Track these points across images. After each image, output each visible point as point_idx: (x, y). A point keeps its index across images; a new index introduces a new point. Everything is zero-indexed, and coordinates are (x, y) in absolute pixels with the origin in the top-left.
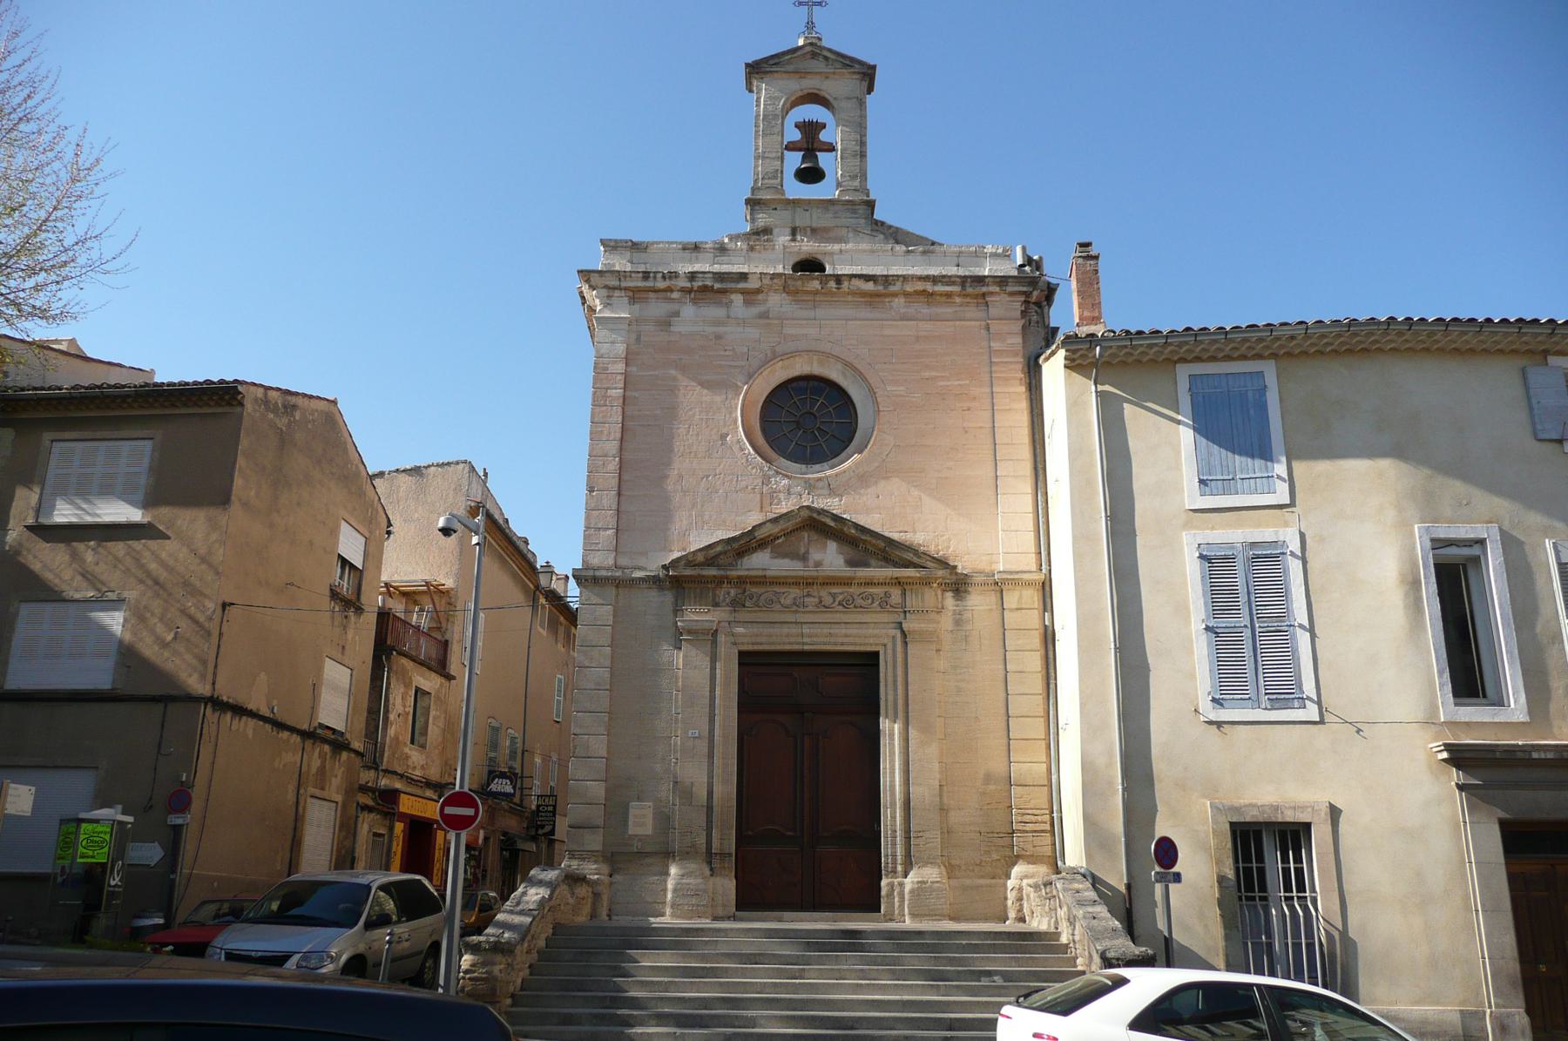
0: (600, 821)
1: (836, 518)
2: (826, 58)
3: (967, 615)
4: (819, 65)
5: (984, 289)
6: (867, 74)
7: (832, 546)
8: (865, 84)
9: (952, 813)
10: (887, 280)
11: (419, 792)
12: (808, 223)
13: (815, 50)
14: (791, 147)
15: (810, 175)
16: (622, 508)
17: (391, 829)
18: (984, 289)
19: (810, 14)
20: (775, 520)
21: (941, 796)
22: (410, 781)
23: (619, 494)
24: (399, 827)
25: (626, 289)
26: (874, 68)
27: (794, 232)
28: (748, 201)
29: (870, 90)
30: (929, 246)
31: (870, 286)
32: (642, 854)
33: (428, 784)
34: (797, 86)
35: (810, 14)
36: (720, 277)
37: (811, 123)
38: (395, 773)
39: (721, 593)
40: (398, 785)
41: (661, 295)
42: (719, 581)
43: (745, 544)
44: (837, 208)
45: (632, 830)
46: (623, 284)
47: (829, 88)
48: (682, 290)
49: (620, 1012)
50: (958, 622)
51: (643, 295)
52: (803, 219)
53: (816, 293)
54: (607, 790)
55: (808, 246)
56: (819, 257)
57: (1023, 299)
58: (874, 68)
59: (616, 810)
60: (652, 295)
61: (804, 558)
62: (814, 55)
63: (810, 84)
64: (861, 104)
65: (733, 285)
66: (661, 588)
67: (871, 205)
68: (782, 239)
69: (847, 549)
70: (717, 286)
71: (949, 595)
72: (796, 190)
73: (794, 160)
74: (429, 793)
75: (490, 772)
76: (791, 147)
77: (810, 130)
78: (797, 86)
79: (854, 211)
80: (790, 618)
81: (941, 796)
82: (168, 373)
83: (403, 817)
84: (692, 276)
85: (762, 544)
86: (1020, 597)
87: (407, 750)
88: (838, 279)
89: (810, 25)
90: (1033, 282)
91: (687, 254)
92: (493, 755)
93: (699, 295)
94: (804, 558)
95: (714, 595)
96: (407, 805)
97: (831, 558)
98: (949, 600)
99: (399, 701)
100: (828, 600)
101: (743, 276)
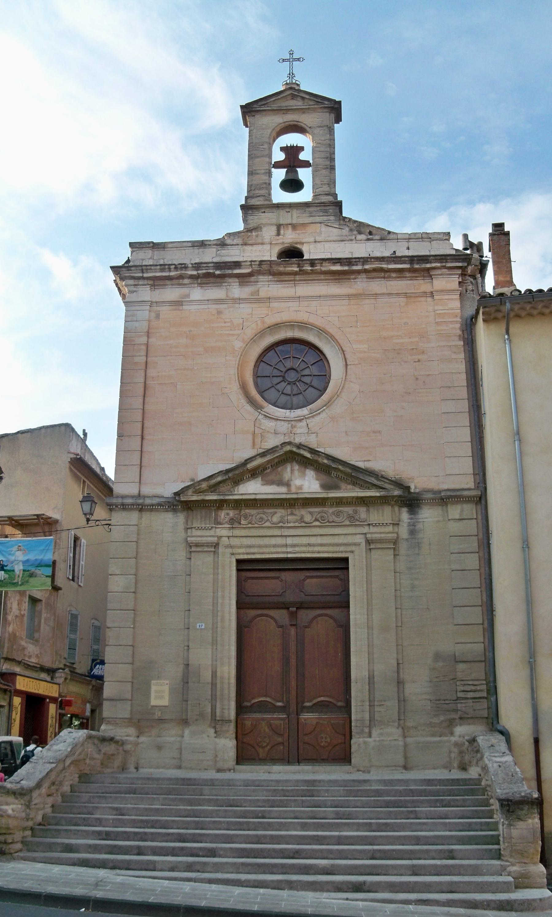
0: (129, 696)
1: (313, 451)
2: (303, 98)
3: (419, 526)
4: (297, 103)
5: (428, 266)
6: (335, 109)
7: (310, 474)
8: (333, 116)
9: (407, 686)
10: (349, 261)
11: (34, 675)
12: (289, 221)
13: (293, 91)
14: (278, 165)
15: (292, 184)
16: (145, 449)
17: (10, 704)
18: (428, 266)
19: (291, 68)
20: (263, 455)
21: (398, 672)
22: (28, 666)
23: (142, 439)
24: (17, 701)
25: (148, 278)
26: (339, 103)
27: (279, 227)
28: (243, 207)
29: (338, 119)
30: (385, 236)
31: (338, 268)
32: (161, 721)
33: (42, 669)
34: (278, 120)
35: (291, 68)
36: (219, 265)
37: (292, 147)
38: (13, 660)
39: (222, 514)
40: (17, 669)
41: (175, 282)
42: (221, 504)
43: (238, 474)
44: (311, 209)
45: (154, 702)
46: (145, 275)
47: (305, 119)
48: (191, 277)
49: (395, 788)
50: (413, 532)
51: (161, 282)
52: (285, 217)
53: (295, 274)
54: (133, 671)
55: (289, 237)
56: (299, 246)
57: (460, 272)
58: (339, 103)
59: (140, 684)
60: (168, 282)
61: (280, 483)
62: (293, 97)
63: (290, 118)
64: (331, 131)
65: (230, 272)
66: (175, 511)
67: (339, 205)
68: (268, 233)
69: (323, 477)
70: (218, 272)
71: (405, 510)
72: (280, 196)
73: (279, 175)
74: (44, 675)
75: (93, 660)
76: (278, 165)
77: (292, 152)
78: (278, 120)
79: (326, 211)
80: (277, 532)
81: (398, 672)
82: (95, 454)
83: (19, 693)
84: (197, 266)
85: (254, 474)
86: (462, 511)
87: (23, 643)
88: (312, 262)
89: (291, 75)
90: (467, 259)
91: (196, 250)
92: (95, 647)
93: (204, 280)
94: (288, 485)
95: (216, 516)
96: (22, 684)
97: (308, 483)
98: (405, 515)
99: (15, 606)
100: (308, 518)
101: (237, 265)
